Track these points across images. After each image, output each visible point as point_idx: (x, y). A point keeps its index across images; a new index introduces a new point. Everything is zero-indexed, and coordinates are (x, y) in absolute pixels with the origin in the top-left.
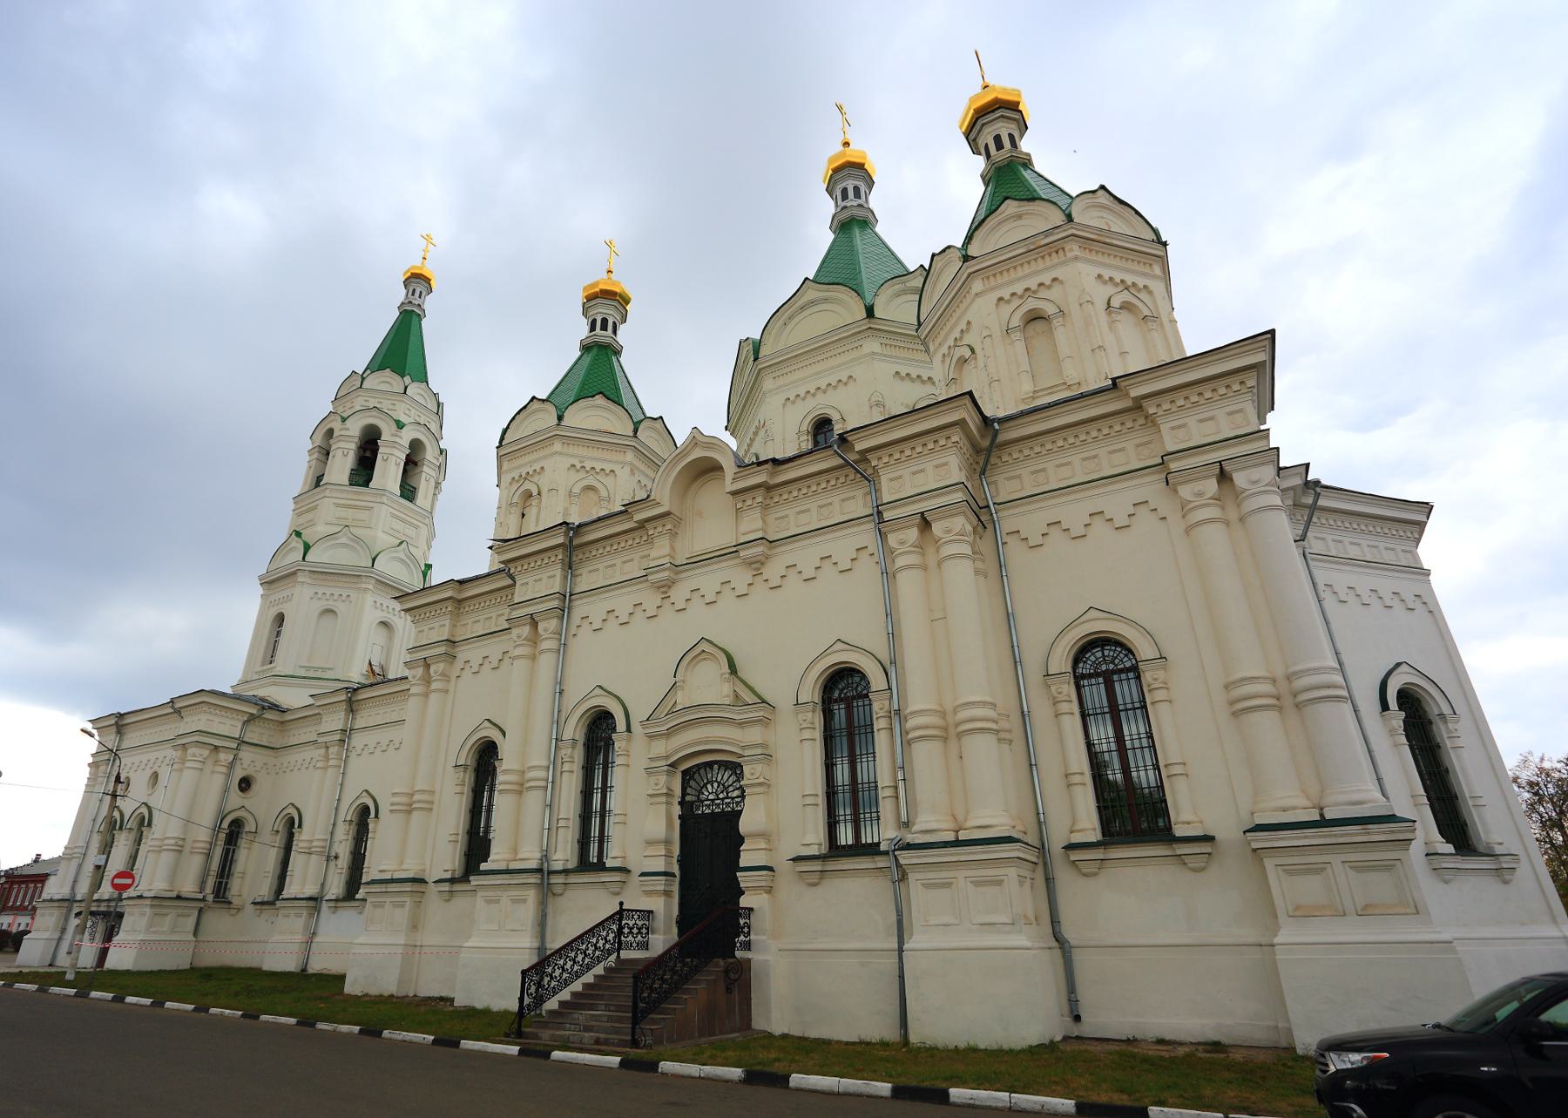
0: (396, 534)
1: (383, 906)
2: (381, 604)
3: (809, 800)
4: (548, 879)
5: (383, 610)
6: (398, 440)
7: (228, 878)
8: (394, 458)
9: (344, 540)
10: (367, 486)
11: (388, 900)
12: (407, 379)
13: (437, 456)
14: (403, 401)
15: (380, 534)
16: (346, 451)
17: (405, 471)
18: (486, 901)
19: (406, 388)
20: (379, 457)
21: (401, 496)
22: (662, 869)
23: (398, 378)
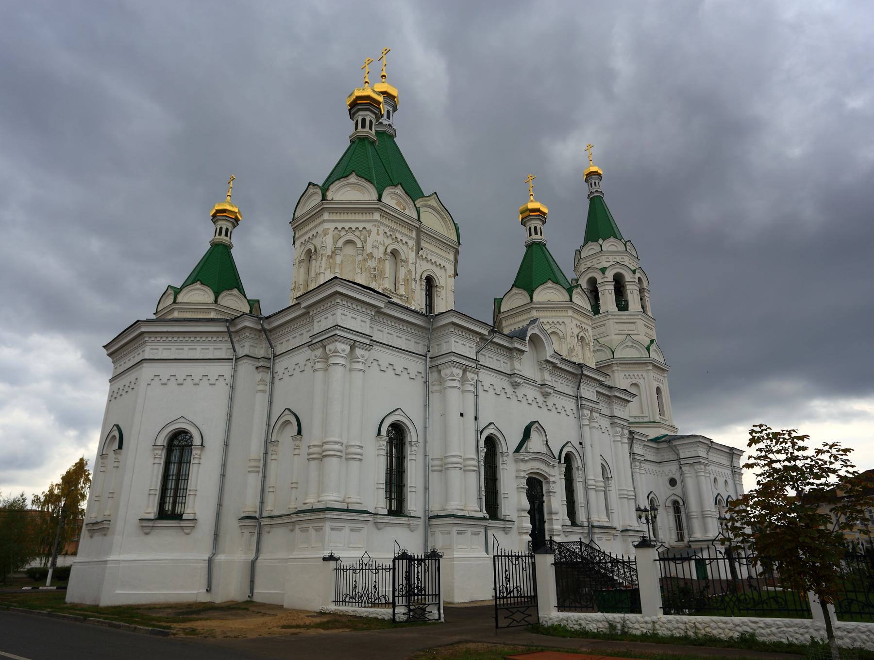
0: (622, 333)
1: (307, 531)
2: (633, 375)
3: (413, 489)
4: (591, 530)
5: (631, 378)
6: (606, 280)
7: (678, 533)
8: (607, 291)
9: (629, 343)
10: (599, 313)
11: (311, 526)
12: (600, 241)
13: (632, 276)
14: (602, 256)
15: (614, 337)
16: (631, 291)
18: (315, 529)
19: (601, 246)
20: (600, 293)
23: (595, 243)
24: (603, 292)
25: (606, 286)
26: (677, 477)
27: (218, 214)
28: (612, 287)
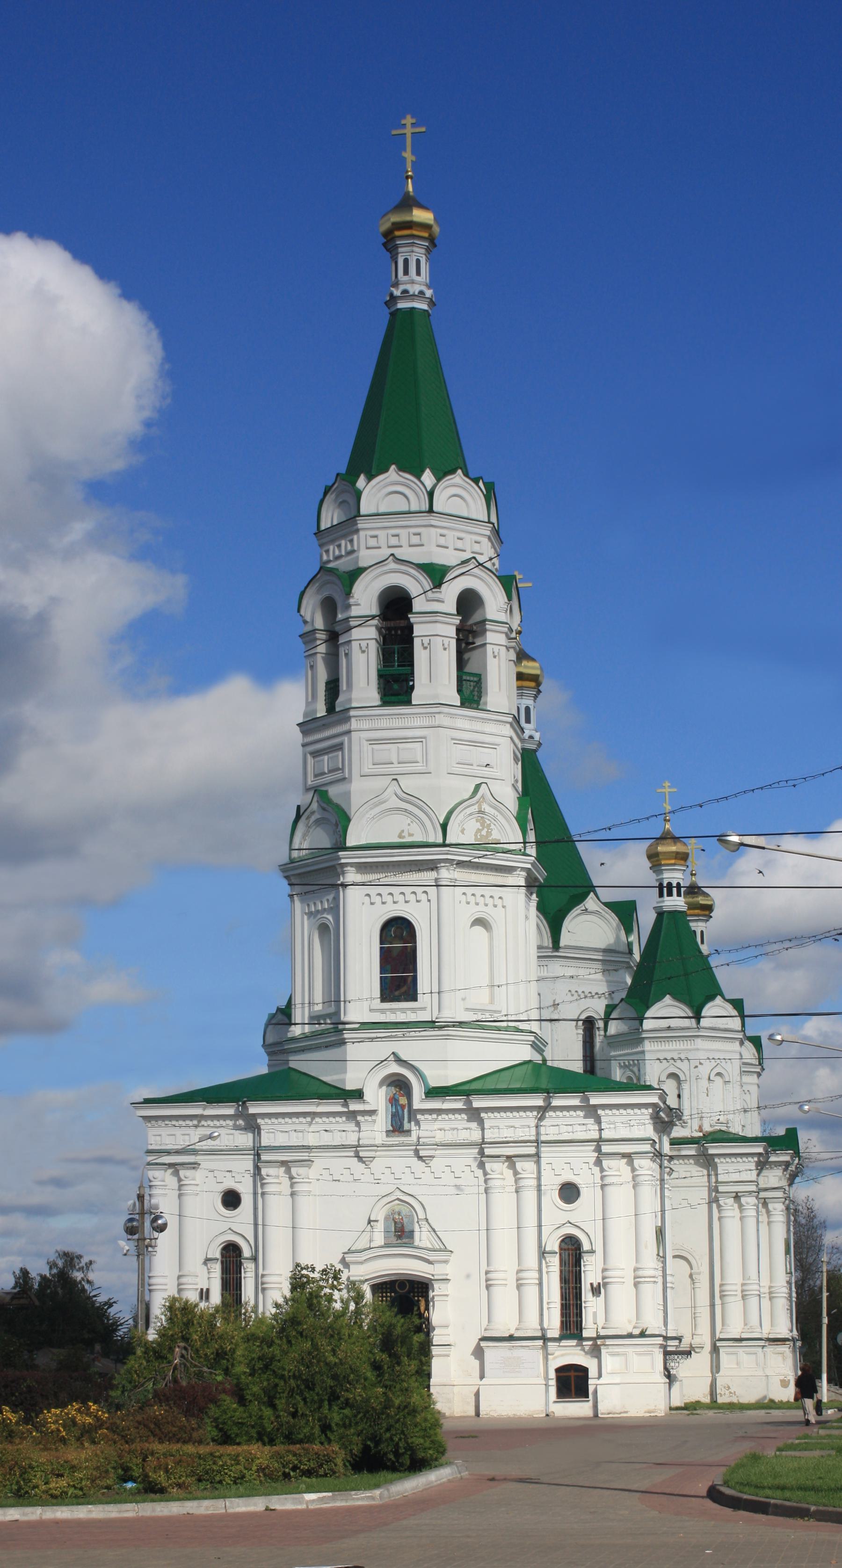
8: (439, 639)
12: (428, 478)
16: (364, 644)
17: (460, 653)
19: (431, 494)
20: (417, 642)
21: (463, 705)
22: (537, 1288)
24: (426, 640)
25: (439, 625)
26: (245, 1189)
27: (397, 233)
28: (452, 631)
